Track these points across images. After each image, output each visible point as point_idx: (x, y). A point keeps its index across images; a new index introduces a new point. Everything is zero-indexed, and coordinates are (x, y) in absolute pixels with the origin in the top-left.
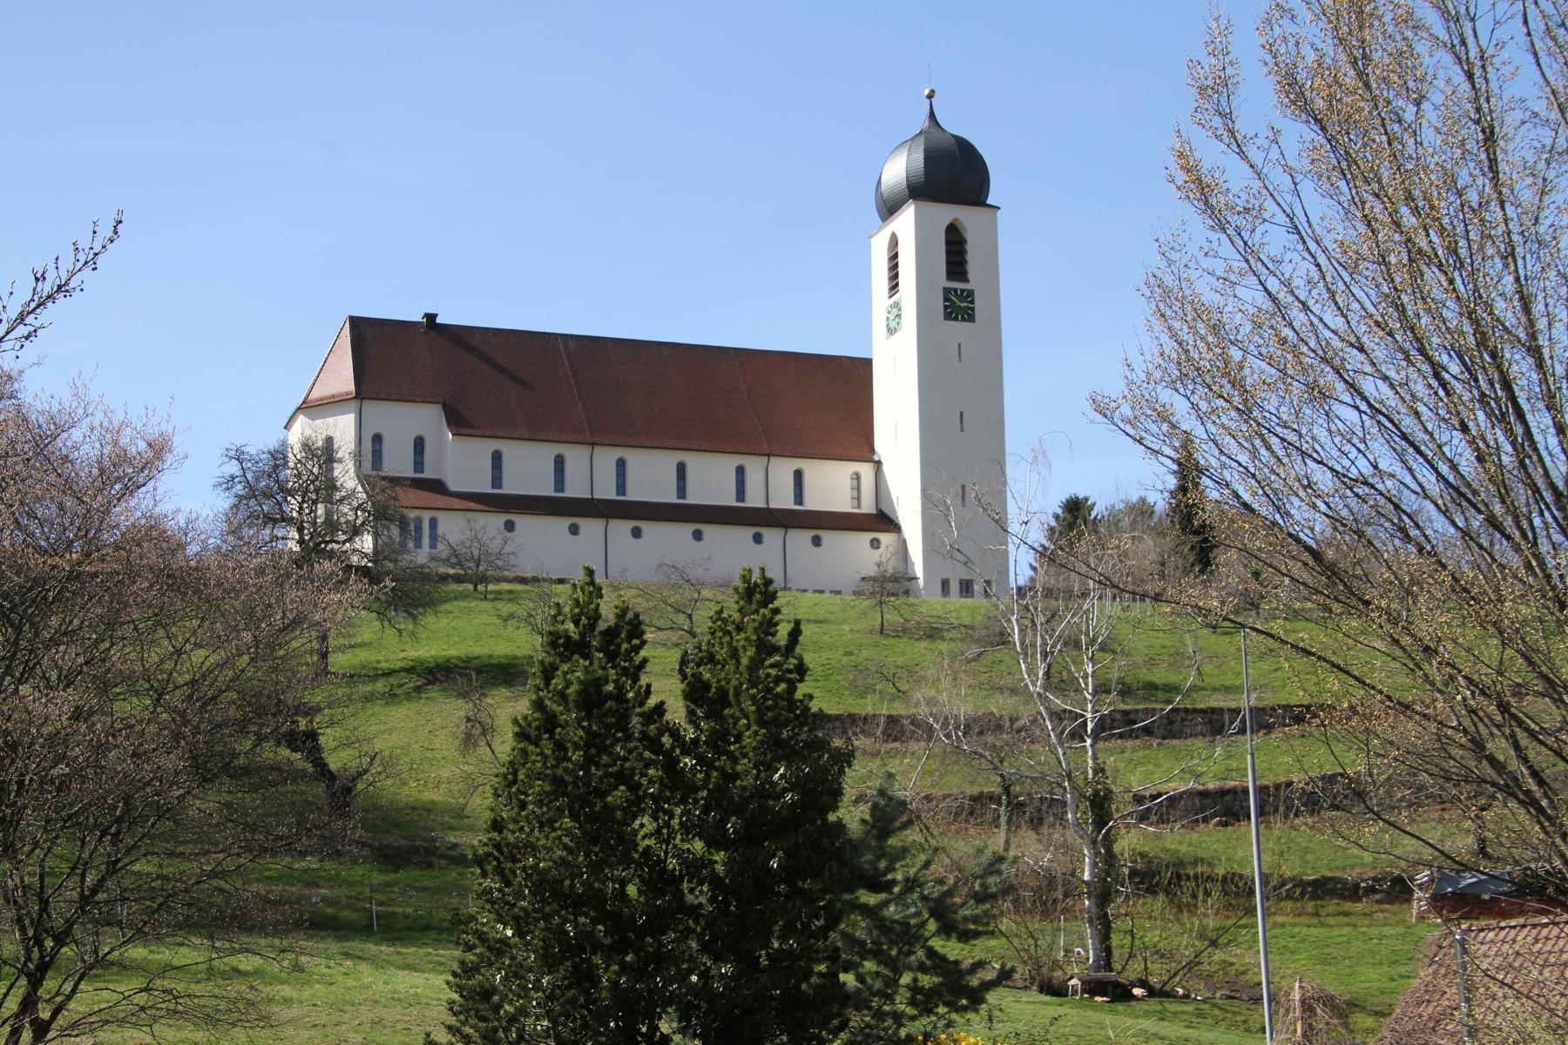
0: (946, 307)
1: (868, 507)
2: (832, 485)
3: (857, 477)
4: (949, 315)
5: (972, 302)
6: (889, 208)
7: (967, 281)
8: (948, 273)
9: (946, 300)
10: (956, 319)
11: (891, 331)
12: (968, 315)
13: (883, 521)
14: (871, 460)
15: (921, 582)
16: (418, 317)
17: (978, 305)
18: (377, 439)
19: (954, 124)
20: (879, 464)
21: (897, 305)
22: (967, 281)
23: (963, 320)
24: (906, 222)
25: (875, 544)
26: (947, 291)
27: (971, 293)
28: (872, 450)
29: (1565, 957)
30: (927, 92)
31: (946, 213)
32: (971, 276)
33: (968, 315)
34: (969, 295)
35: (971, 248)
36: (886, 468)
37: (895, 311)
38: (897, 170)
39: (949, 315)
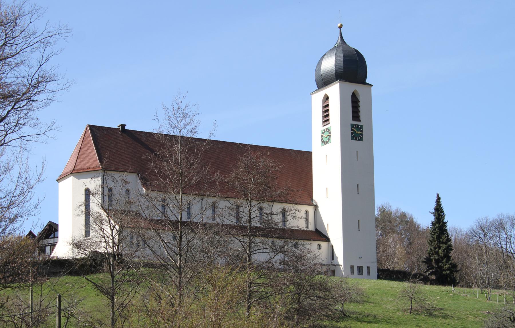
0: (352, 134)
1: (311, 228)
2: (298, 218)
3: (307, 212)
4: (353, 138)
5: (362, 131)
6: (324, 82)
7: (360, 121)
8: (353, 116)
9: (352, 130)
10: (356, 139)
11: (324, 143)
12: (361, 139)
13: (320, 235)
14: (313, 205)
15: (342, 268)
16: (115, 125)
17: (364, 133)
18: (110, 190)
19: (352, 43)
20: (316, 207)
21: (328, 130)
22: (360, 121)
23: (359, 140)
24: (334, 91)
25: (320, 246)
26: (352, 126)
27: (361, 127)
28: (312, 199)
29: (98, 326)
30: (339, 25)
31: (352, 87)
32: (361, 118)
33: (361, 139)
34: (360, 128)
35: (361, 104)
36: (320, 209)
37: (327, 134)
38: (329, 64)
39: (353, 138)
